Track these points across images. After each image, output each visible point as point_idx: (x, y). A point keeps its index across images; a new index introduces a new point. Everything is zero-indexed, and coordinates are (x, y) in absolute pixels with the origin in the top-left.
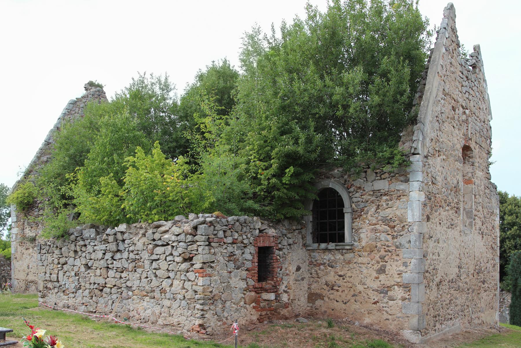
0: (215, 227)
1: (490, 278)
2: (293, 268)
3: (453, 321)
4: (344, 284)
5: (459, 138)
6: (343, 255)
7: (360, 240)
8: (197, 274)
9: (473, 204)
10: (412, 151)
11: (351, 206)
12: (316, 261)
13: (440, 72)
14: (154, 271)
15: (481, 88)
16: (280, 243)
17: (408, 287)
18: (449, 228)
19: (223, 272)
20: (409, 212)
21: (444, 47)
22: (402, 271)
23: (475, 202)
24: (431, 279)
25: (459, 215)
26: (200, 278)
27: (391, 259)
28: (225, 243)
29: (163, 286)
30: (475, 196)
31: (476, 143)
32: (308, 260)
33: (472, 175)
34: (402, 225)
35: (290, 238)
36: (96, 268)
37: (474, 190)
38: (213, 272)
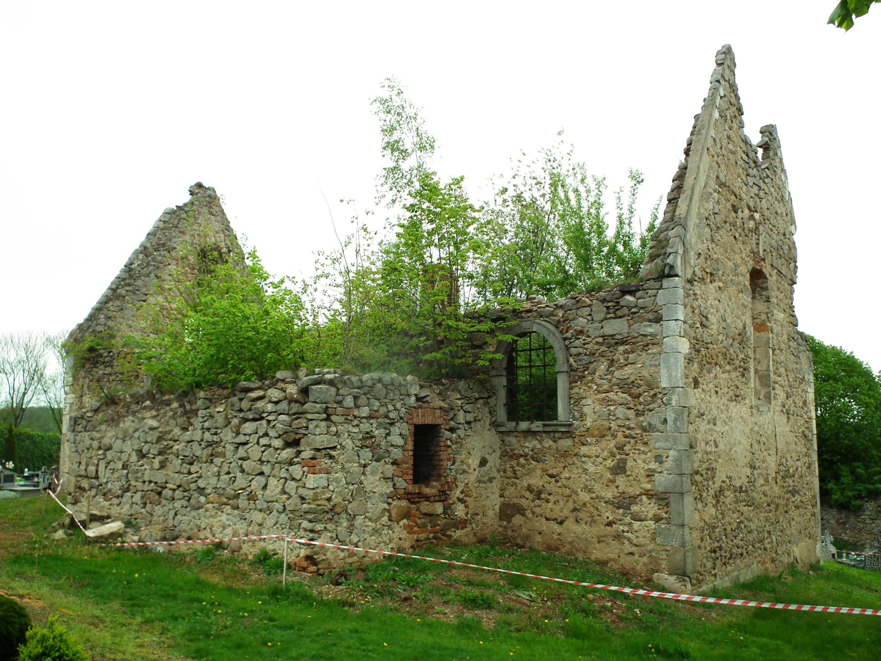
0: (338, 389)
1: (804, 485)
2: (474, 462)
3: (745, 558)
4: (557, 489)
5: (744, 256)
6: (555, 442)
7: (583, 416)
8: (306, 469)
9: (771, 363)
10: (666, 272)
11: (568, 361)
12: (512, 450)
13: (710, 148)
14: (240, 462)
15: (778, 182)
16: (452, 419)
17: (665, 499)
18: (731, 401)
19: (350, 465)
20: (663, 372)
21: (717, 110)
22: (654, 471)
23: (774, 360)
24: (704, 486)
25: (748, 380)
26: (309, 475)
27: (635, 449)
28: (355, 417)
29: (253, 487)
30: (774, 350)
31: (772, 266)
32: (500, 448)
33: (768, 317)
34: (652, 393)
35: (469, 412)
36: (153, 456)
37: (771, 342)
38: (332, 465)
